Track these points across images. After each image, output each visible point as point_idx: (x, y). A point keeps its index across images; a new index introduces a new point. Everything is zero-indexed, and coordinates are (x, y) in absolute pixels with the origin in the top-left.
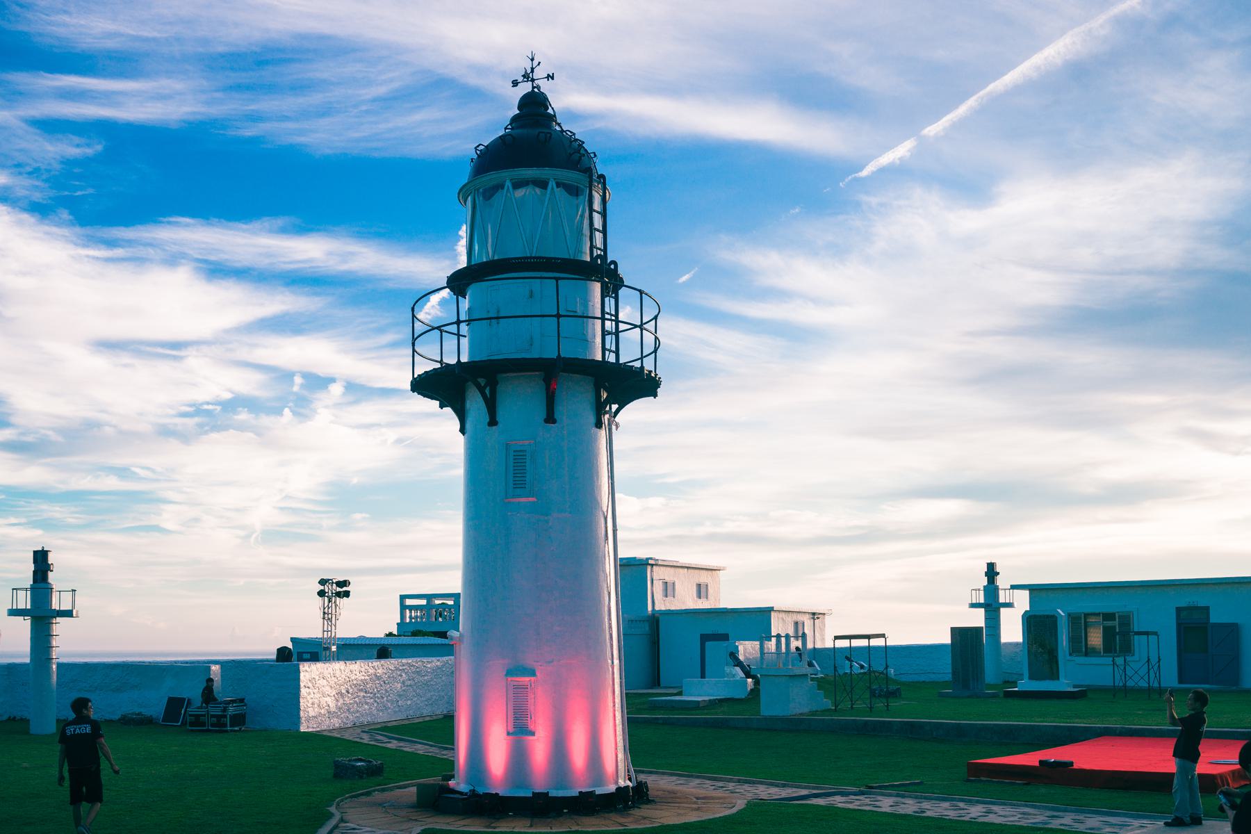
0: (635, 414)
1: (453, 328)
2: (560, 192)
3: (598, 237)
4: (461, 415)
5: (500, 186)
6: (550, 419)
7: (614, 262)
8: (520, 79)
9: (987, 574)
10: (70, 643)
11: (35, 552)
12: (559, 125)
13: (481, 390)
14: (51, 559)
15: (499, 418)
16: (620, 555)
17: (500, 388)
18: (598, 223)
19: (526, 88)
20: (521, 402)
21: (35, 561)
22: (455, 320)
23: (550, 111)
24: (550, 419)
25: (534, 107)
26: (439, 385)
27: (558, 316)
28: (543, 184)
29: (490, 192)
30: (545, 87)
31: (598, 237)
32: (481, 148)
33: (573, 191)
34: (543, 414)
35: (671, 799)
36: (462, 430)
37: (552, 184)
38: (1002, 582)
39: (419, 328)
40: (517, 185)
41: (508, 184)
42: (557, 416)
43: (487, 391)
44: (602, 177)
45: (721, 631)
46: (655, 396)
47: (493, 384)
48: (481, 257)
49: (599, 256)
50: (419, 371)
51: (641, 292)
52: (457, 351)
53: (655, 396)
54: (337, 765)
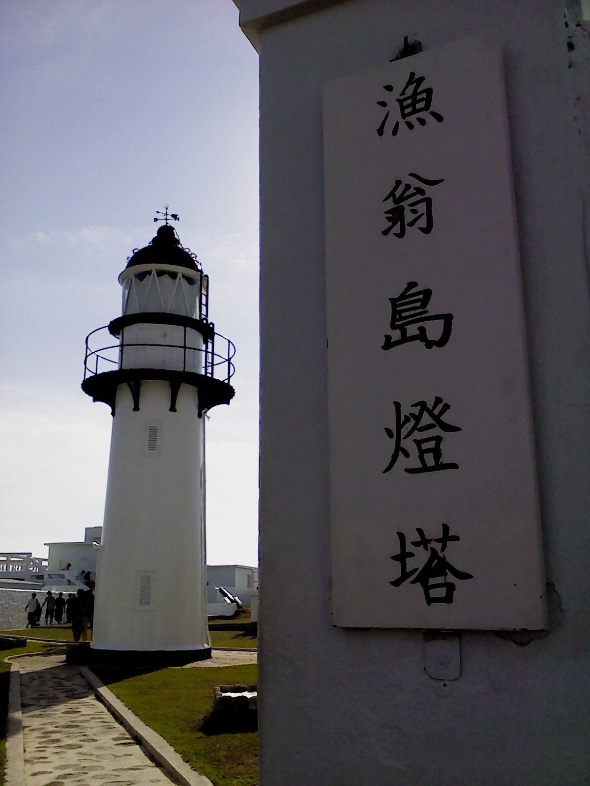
0: (216, 412)
2: (184, 282)
3: (204, 308)
5: (149, 273)
6: (173, 409)
7: (212, 323)
8: (573, 55)
12: (181, 245)
13: (131, 388)
18: (204, 302)
20: (155, 396)
23: (180, 246)
25: (166, 235)
26: (99, 387)
28: (173, 275)
29: (141, 276)
30: (172, 223)
31: (204, 308)
32: (136, 251)
33: (190, 281)
36: (113, 414)
37: (180, 275)
39: (89, 352)
40: (160, 273)
41: (154, 272)
42: (177, 407)
44: (206, 276)
46: (228, 404)
48: (134, 310)
49: (204, 319)
50: (87, 376)
51: (229, 342)
52: (109, 363)
53: (228, 404)
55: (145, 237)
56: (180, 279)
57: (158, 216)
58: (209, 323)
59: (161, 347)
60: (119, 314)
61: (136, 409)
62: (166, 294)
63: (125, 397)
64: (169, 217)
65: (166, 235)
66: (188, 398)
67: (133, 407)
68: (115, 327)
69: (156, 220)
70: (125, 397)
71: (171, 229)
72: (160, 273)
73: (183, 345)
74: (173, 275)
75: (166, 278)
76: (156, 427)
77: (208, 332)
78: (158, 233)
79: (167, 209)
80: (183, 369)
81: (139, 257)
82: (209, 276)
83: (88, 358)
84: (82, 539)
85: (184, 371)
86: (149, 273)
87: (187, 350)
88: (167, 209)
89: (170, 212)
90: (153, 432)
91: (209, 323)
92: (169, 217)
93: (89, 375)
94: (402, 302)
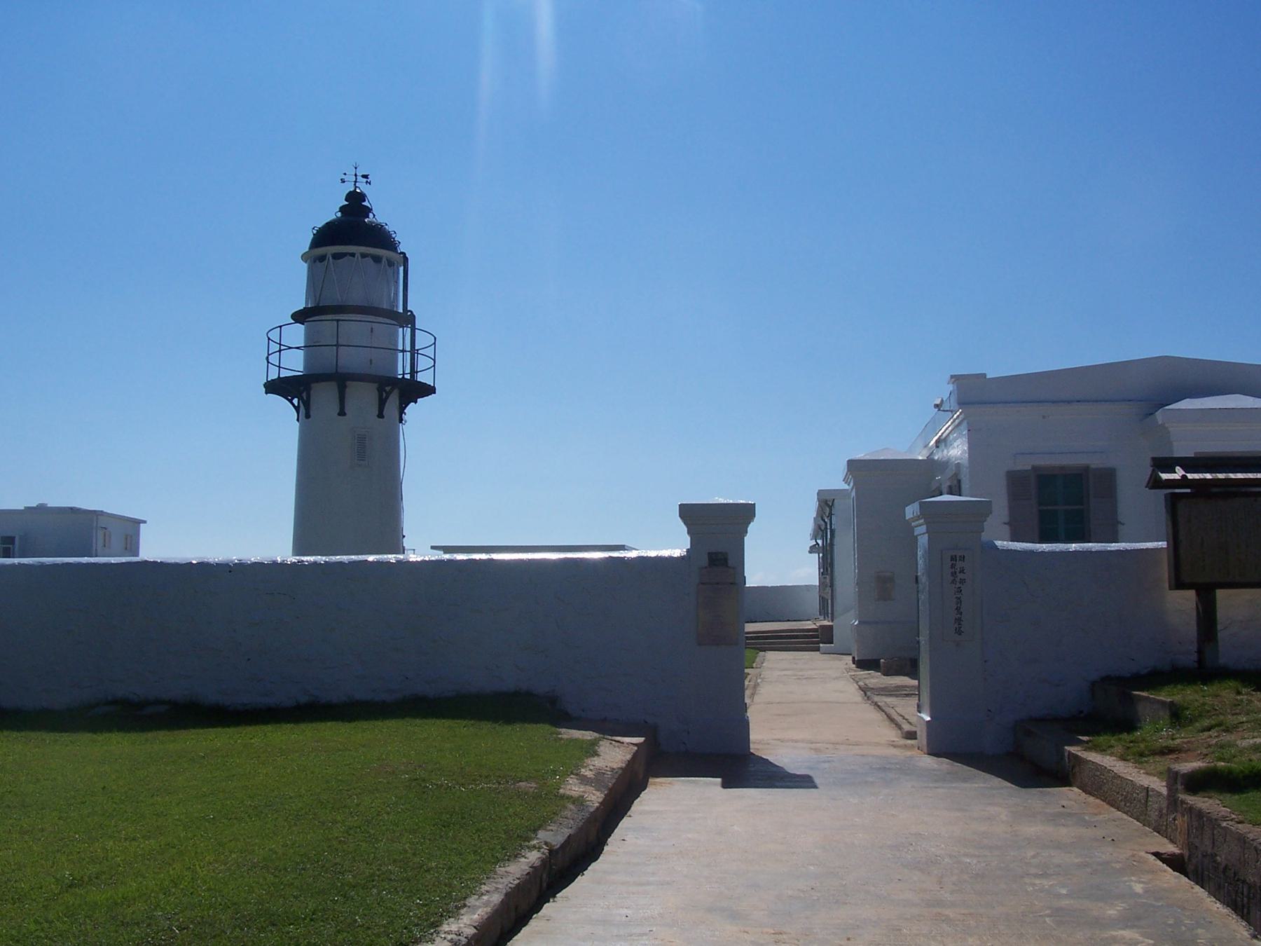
25: (356, 204)
27: (337, 345)
28: (377, 259)
30: (362, 187)
40: (337, 256)
52: (294, 364)
55: (329, 210)
59: (356, 343)
61: (342, 413)
63: (324, 396)
65: (356, 204)
66: (362, 397)
68: (299, 317)
70: (324, 396)
72: (364, 256)
75: (369, 260)
77: (408, 319)
81: (326, 236)
86: (353, 255)
93: (273, 376)
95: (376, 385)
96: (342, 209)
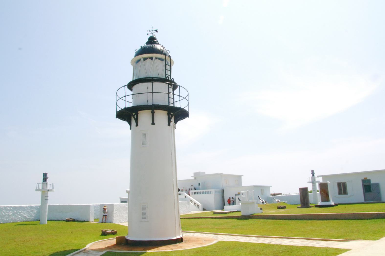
1: (124, 98)
4: (130, 123)
6: (153, 123)
7: (173, 79)
9: (312, 173)
10: (54, 200)
11: (44, 174)
14: (48, 176)
15: (139, 124)
16: (363, 201)
17: (139, 115)
19: (150, 35)
21: (44, 176)
22: (126, 97)
24: (153, 123)
25: (152, 40)
26: (127, 115)
28: (151, 58)
33: (161, 59)
34: (151, 122)
35: (190, 241)
36: (131, 129)
38: (316, 175)
40: (145, 59)
42: (155, 122)
43: (135, 116)
45: (299, 209)
47: (137, 114)
50: (118, 110)
54: (102, 231)
55: (143, 42)
56: (154, 60)
57: (149, 32)
58: (171, 78)
60: (130, 79)
62: (154, 68)
64: (154, 32)
65: (152, 40)
67: (152, 123)
68: (131, 86)
69: (148, 34)
71: (155, 39)
72: (145, 59)
73: (126, 95)
74: (151, 58)
75: (149, 60)
76: (146, 133)
78: (148, 40)
79: (152, 28)
80: (152, 104)
82: (171, 56)
83: (187, 95)
84: (128, 193)
85: (125, 108)
87: (152, 94)
88: (152, 28)
89: (154, 29)
90: (144, 136)
91: (171, 78)
92: (153, 32)
93: (119, 109)
94: (377, 212)
95: (151, 111)
96: (147, 43)
